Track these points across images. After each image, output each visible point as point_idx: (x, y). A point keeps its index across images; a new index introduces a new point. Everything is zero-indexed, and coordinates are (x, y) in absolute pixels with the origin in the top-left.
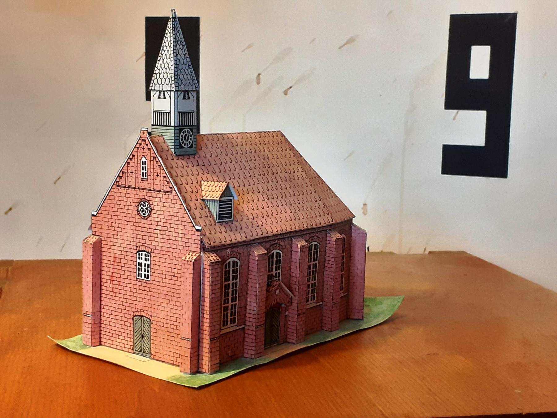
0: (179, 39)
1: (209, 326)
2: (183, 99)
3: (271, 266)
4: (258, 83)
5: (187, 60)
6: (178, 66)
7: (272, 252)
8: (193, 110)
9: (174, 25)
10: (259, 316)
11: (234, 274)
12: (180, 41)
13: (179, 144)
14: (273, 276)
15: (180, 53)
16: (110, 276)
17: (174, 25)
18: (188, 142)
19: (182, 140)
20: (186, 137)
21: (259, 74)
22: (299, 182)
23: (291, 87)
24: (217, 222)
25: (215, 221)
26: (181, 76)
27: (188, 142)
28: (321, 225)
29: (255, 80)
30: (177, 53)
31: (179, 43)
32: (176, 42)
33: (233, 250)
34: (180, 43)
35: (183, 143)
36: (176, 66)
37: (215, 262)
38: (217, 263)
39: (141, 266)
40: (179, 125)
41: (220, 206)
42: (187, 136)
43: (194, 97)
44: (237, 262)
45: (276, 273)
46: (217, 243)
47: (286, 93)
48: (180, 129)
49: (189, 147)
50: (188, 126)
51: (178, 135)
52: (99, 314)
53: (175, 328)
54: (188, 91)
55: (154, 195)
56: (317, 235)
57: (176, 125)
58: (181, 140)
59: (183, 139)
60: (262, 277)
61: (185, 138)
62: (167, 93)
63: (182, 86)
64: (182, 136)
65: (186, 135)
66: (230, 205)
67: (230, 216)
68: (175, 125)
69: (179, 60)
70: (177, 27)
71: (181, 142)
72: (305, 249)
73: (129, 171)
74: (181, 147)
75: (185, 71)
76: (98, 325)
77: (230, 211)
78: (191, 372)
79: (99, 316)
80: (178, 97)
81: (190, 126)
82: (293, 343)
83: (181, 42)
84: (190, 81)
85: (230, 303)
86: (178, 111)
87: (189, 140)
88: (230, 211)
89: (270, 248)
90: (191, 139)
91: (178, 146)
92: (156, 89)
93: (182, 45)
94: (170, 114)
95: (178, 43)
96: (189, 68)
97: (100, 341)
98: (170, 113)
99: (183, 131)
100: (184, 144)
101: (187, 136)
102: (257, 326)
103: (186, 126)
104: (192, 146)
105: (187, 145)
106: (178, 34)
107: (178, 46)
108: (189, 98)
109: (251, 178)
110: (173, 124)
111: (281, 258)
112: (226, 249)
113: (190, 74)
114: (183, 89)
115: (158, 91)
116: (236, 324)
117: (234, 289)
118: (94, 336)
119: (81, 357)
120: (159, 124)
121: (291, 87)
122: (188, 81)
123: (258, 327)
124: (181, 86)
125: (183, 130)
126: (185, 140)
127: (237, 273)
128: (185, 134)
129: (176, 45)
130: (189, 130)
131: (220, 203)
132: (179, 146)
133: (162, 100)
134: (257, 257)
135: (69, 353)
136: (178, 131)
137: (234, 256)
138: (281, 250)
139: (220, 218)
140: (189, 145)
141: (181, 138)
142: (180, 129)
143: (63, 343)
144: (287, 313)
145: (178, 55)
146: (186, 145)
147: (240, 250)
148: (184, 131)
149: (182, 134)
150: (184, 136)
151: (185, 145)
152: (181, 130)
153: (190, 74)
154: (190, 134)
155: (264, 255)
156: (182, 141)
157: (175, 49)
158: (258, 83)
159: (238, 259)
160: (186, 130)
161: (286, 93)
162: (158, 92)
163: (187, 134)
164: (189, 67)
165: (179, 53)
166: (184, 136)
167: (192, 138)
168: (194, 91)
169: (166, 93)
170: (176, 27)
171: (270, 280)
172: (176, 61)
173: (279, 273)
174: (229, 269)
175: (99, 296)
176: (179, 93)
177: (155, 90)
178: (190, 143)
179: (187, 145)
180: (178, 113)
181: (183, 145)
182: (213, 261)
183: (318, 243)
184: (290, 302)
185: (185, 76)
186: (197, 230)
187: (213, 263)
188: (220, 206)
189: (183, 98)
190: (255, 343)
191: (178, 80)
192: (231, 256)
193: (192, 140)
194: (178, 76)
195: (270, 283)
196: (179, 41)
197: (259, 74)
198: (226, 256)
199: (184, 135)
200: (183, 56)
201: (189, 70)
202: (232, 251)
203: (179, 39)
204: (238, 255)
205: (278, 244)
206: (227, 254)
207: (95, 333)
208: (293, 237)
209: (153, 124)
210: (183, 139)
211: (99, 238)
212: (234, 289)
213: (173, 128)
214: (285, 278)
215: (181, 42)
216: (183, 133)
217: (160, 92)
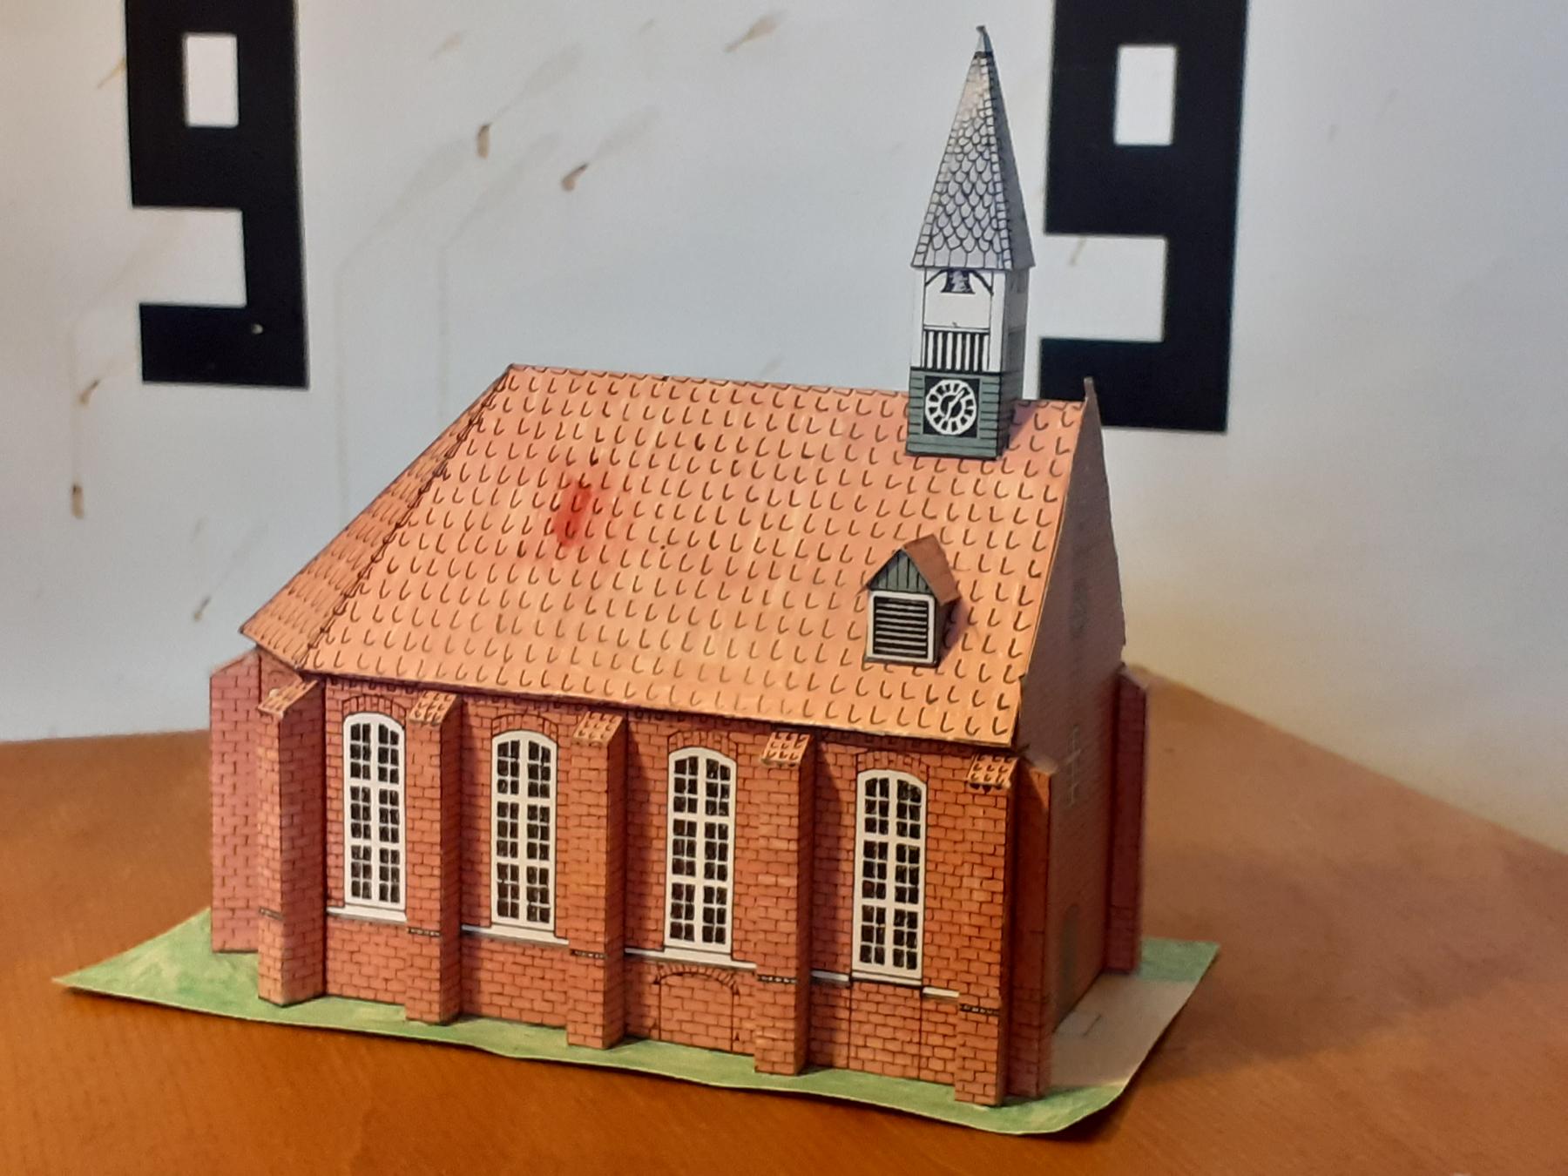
1: (441, 910)
2: (944, 291)
4: (482, 151)
8: (987, 326)
13: (921, 421)
16: (826, 836)
20: (951, 405)
21: (485, 129)
27: (958, 419)
29: (473, 146)
35: (937, 420)
39: (366, 738)
47: (568, 183)
49: (964, 435)
50: (962, 371)
51: (921, 393)
54: (966, 272)
65: (951, 398)
74: (928, 429)
86: (924, 325)
91: (918, 424)
92: (937, 265)
94: (986, 338)
98: (989, 334)
103: (953, 370)
104: (971, 432)
105: (954, 427)
108: (968, 289)
114: (941, 263)
115: (941, 272)
119: (645, 1082)
135: (168, 1013)
136: (922, 384)
140: (961, 429)
143: (96, 978)
151: (945, 426)
152: (931, 382)
158: (482, 151)
163: (951, 398)
168: (992, 271)
169: (972, 278)
176: (930, 274)
177: (933, 267)
180: (924, 330)
182: (981, 781)
189: (942, 287)
197: (485, 129)
209: (918, 365)
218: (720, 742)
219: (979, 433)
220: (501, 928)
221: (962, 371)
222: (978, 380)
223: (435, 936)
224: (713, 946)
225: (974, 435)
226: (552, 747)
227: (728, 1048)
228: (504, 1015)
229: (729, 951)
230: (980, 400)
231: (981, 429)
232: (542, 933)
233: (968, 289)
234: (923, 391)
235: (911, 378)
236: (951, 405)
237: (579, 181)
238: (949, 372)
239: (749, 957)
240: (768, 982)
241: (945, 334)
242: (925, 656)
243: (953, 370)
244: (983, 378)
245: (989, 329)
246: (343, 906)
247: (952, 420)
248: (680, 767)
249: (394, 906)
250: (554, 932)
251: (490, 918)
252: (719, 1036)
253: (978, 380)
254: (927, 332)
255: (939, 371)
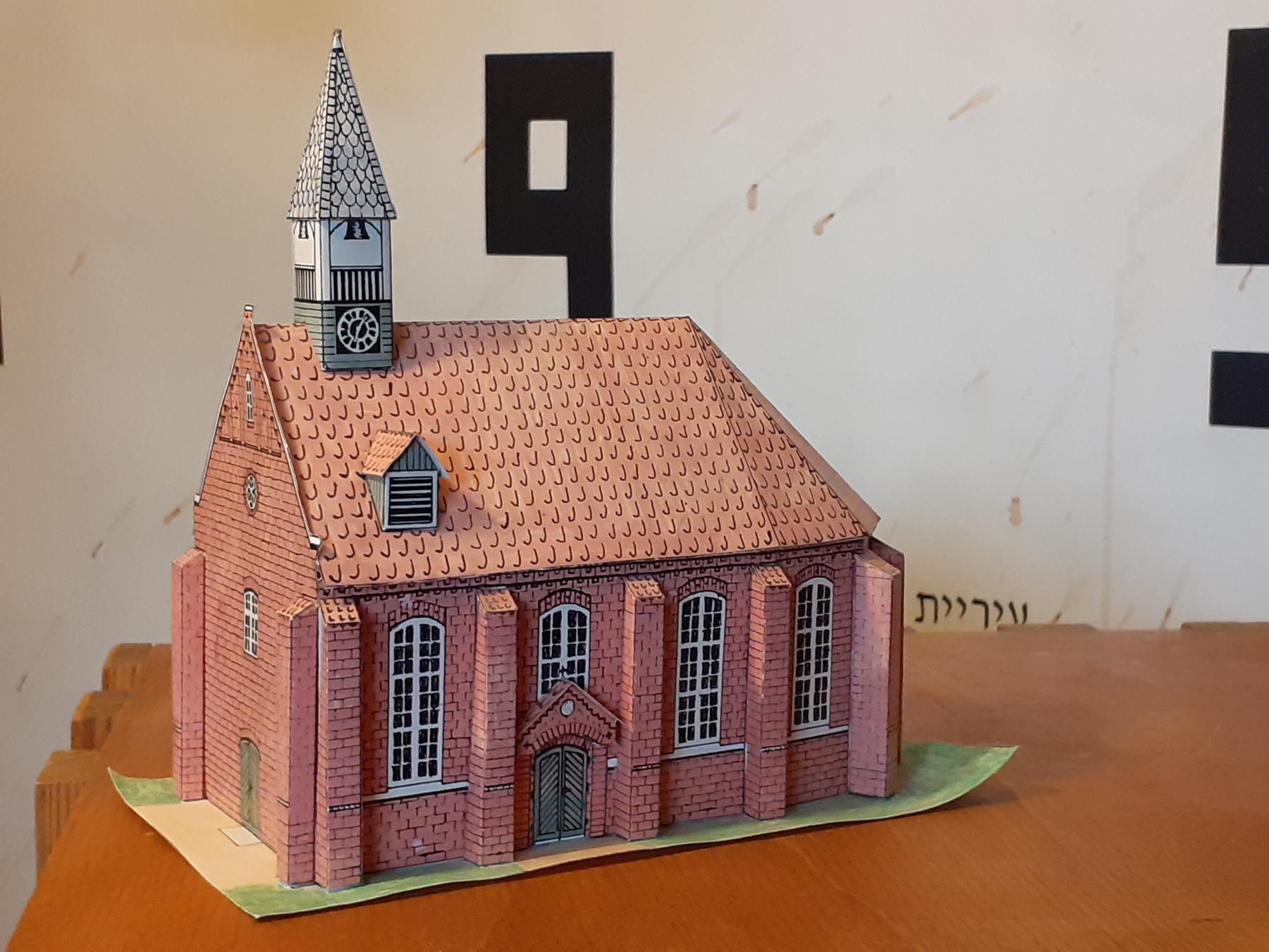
0: (345, 99)
2: (346, 238)
3: (820, 662)
4: (752, 206)
5: (365, 146)
6: (335, 160)
7: (556, 610)
8: (380, 264)
9: (335, 66)
10: (495, 764)
11: (549, 658)
12: (349, 104)
14: (561, 668)
15: (346, 128)
17: (335, 66)
18: (363, 340)
19: (344, 333)
20: (358, 329)
21: (755, 186)
22: (698, 447)
23: (832, 216)
24: (384, 529)
25: (379, 528)
26: (342, 186)
27: (363, 340)
28: (728, 551)
30: (337, 132)
31: (345, 108)
32: (335, 106)
33: (419, 598)
34: (349, 107)
35: (347, 341)
36: (328, 161)
37: (342, 625)
38: (347, 627)
40: (333, 299)
41: (392, 492)
42: (361, 324)
43: (381, 234)
44: (435, 628)
45: (571, 664)
46: (363, 580)
48: (336, 307)
49: (369, 351)
50: (364, 301)
52: (202, 728)
53: (647, 793)
54: (362, 221)
55: (267, 462)
56: (715, 574)
57: (327, 298)
58: (343, 336)
59: (349, 331)
60: (499, 669)
61: (355, 330)
62: (372, 225)
63: (343, 208)
64: (344, 325)
65: (358, 322)
66: (429, 491)
67: (428, 516)
68: (324, 299)
69: (341, 147)
70: (343, 71)
71: (342, 339)
72: (652, 609)
73: (234, 406)
74: (341, 350)
75: (355, 174)
76: (200, 753)
77: (429, 506)
78: (291, 881)
79: (200, 734)
80: (330, 233)
81: (371, 301)
82: (626, 839)
83: (352, 105)
84: (368, 196)
85: (416, 728)
86: (331, 267)
87: (368, 335)
88: (429, 506)
89: (548, 600)
90: (372, 333)
93: (355, 112)
94: (380, 273)
95: (341, 108)
96: (370, 166)
97: (204, 791)
98: (382, 270)
99: (346, 314)
100: (350, 342)
101: (361, 324)
102: (488, 787)
103: (357, 301)
104: (376, 349)
105: (362, 346)
106: (344, 87)
107: (341, 117)
108: (365, 236)
109: (543, 429)
110: (319, 298)
111: (585, 625)
112: (400, 594)
113: (373, 180)
116: (438, 777)
117: (426, 693)
118: (188, 776)
120: (360, 298)
121: (832, 216)
122: (361, 198)
123: (491, 789)
124: (338, 207)
125: (375, 316)
126: (353, 334)
127: (438, 653)
128: (353, 320)
129: (336, 113)
130: (367, 312)
131: (393, 486)
132: (335, 349)
133: (357, 243)
134: (483, 619)
136: (333, 314)
137: (426, 614)
138: (588, 607)
139: (391, 520)
140: (367, 348)
141: (340, 329)
142: (336, 307)
144: (612, 763)
145: (337, 135)
146: (358, 346)
147: (446, 599)
148: (350, 312)
149: (343, 319)
150: (349, 326)
151: (354, 345)
153: (373, 180)
154: (370, 321)
155: (506, 615)
156: (345, 337)
157: (333, 123)
158: (752, 206)
159: (438, 621)
160: (357, 311)
161: (818, 230)
162: (346, 224)
163: (358, 322)
164: (369, 161)
165: (356, 137)
166: (349, 326)
167: (376, 330)
169: (367, 226)
170: (340, 71)
171: (551, 679)
172: (331, 149)
173: (825, 679)
174: (409, 644)
175: (201, 687)
176: (334, 223)
178: (369, 341)
179: (362, 346)
180: (331, 271)
181: (348, 346)
182: (337, 621)
183: (719, 595)
184: (614, 736)
185: (355, 185)
186: (313, 547)
187: (334, 626)
188: (392, 492)
189: (345, 234)
190: (484, 828)
191: (332, 194)
192: (416, 613)
193: (377, 335)
194: (333, 185)
195: (552, 685)
196: (346, 104)
197: (755, 186)
198: (398, 612)
199: (349, 324)
200: (353, 138)
201: (369, 170)
202: (419, 602)
203: (345, 99)
204: (437, 612)
205: (576, 591)
206: (401, 607)
207: (190, 770)
208: (627, 576)
210: (349, 331)
211: (201, 554)
212: (426, 693)
213: (319, 306)
214: (603, 677)
215: (352, 105)
216: (348, 318)
217: (351, 221)
218: (437, 612)
219: (383, 348)
220: (398, 789)
221: (371, 301)
222: (378, 307)
223: (657, 768)
224: (427, 778)
225: (379, 352)
226: (831, 585)
227: (433, 851)
228: (437, 850)
229: (718, 740)
230: (381, 322)
231: (333, 347)
232: (432, 784)
233: (365, 236)
234: (335, 320)
235: (391, 309)
236: (358, 329)
237: (828, 227)
238: (354, 302)
239: (732, 740)
240: (354, 804)
241: (343, 272)
242: (430, 519)
243: (351, 301)
244: (382, 305)
245: (382, 266)
246: (386, 792)
247: (360, 340)
248: (398, 637)
249: (408, 781)
250: (441, 781)
251: (674, 745)
252: (700, 801)
253: (378, 307)
254: (335, 272)
255: (347, 302)
